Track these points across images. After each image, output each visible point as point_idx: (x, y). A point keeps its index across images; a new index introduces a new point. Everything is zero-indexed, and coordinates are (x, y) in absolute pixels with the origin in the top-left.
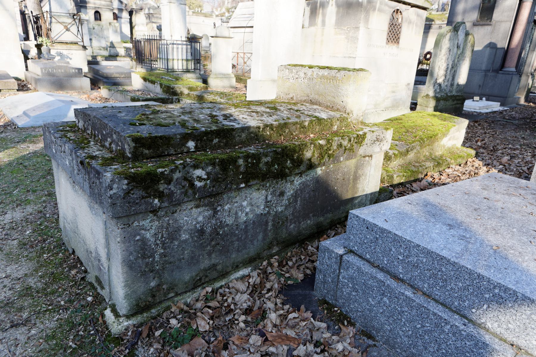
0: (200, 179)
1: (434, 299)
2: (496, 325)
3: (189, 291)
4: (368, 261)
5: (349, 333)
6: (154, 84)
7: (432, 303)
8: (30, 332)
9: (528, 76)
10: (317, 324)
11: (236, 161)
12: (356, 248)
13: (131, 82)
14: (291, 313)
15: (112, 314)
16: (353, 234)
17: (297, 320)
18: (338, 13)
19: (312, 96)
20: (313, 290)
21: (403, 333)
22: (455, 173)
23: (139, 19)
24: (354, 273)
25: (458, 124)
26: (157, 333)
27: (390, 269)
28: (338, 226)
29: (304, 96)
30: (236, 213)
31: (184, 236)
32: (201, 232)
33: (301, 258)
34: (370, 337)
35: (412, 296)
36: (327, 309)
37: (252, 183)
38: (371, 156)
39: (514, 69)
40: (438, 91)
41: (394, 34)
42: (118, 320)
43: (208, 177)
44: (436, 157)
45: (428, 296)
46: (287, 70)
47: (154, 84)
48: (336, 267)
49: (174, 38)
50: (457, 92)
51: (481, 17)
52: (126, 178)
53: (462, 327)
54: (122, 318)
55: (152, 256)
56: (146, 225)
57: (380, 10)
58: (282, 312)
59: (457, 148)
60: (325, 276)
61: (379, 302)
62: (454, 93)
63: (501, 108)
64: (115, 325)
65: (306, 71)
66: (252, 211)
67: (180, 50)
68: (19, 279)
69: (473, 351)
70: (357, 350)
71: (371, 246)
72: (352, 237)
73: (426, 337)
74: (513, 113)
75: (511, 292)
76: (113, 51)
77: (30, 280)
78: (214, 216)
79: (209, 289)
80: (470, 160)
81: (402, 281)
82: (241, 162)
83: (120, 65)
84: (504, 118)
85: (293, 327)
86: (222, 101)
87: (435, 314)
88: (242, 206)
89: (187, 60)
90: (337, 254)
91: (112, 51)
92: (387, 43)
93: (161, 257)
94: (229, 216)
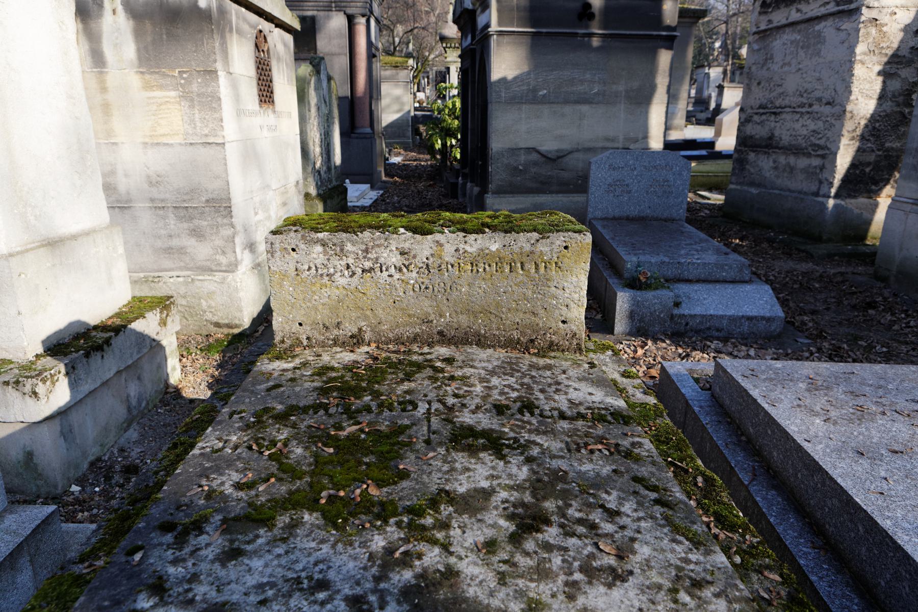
18: (138, 34)
19: (447, 319)
29: (412, 325)
46: (319, 248)
65: (407, 245)
92: (261, 107)
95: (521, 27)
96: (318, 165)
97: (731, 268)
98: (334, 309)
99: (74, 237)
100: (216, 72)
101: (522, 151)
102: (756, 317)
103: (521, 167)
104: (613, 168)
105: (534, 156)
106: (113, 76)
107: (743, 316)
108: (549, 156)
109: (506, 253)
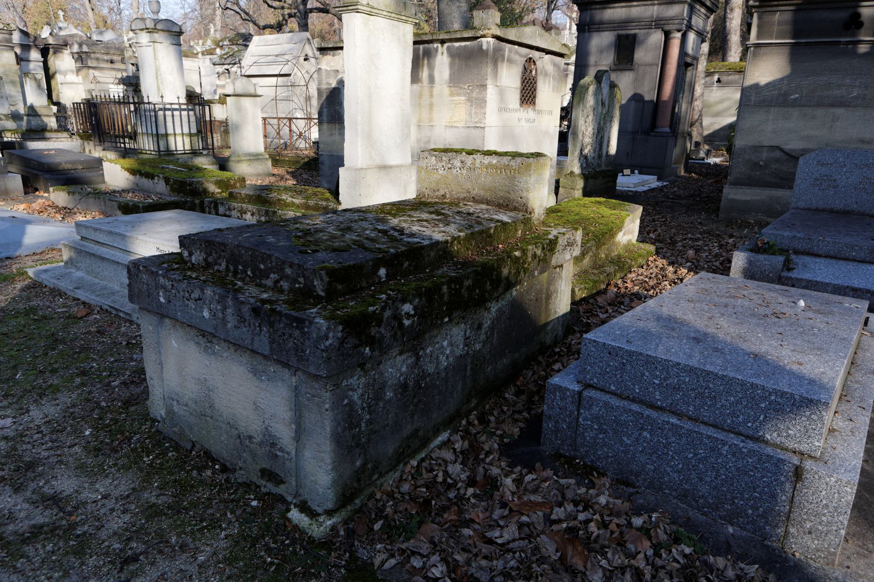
0: (408, 316)
1: (702, 422)
2: (775, 435)
3: (391, 470)
4: (613, 393)
5: (604, 485)
6: (153, 178)
7: (702, 427)
8: (196, 558)
9: (685, 138)
10: (563, 481)
11: (441, 289)
12: (595, 380)
13: (103, 175)
14: (526, 475)
15: (303, 515)
16: (590, 364)
17: (535, 483)
18: (452, 65)
20: (539, 444)
21: (671, 469)
22: (640, 278)
23: (64, 62)
24: (600, 410)
25: (632, 212)
26: (377, 527)
27: (643, 398)
28: (533, 363)
30: (438, 358)
31: (389, 394)
32: (404, 386)
33: (502, 410)
34: (628, 484)
35: (678, 422)
36: (566, 463)
37: (455, 314)
38: (561, 266)
39: (667, 130)
40: (584, 165)
41: (528, 94)
42: (317, 520)
43: (415, 313)
44: (612, 258)
45: (695, 420)
47: (153, 178)
48: (572, 407)
49: (167, 100)
50: (607, 165)
51: (618, 59)
52: (341, 324)
53: (742, 445)
54: (322, 517)
55: (359, 425)
56: (354, 383)
57: (510, 61)
58: (514, 476)
59: (633, 245)
60: (557, 422)
61: (637, 439)
62: (603, 168)
63: (659, 184)
64: (314, 527)
66: (452, 352)
67: (185, 120)
68: (128, 496)
69: (756, 468)
70: (620, 501)
71: (616, 375)
72: (589, 368)
73: (701, 466)
74: (676, 189)
75: (788, 395)
76: (35, 122)
77: (146, 495)
78: (417, 364)
79: (414, 463)
80: (651, 259)
81: (661, 409)
82: (445, 288)
83: (61, 147)
84: (668, 198)
85: (535, 491)
86: (296, 201)
87: (709, 437)
88: (442, 347)
89: (191, 135)
90: (574, 391)
91: (33, 123)
92: (521, 106)
93: (367, 426)
94: (430, 362)
95: (785, 38)
96: (586, 151)
97: (861, 249)
98: (437, 183)
99: (391, 167)
100: (486, 86)
101: (765, 149)
102: (861, 289)
103: (761, 163)
104: (820, 164)
105: (778, 154)
106: (437, 88)
107: (848, 287)
108: (793, 154)
109: (498, 165)
